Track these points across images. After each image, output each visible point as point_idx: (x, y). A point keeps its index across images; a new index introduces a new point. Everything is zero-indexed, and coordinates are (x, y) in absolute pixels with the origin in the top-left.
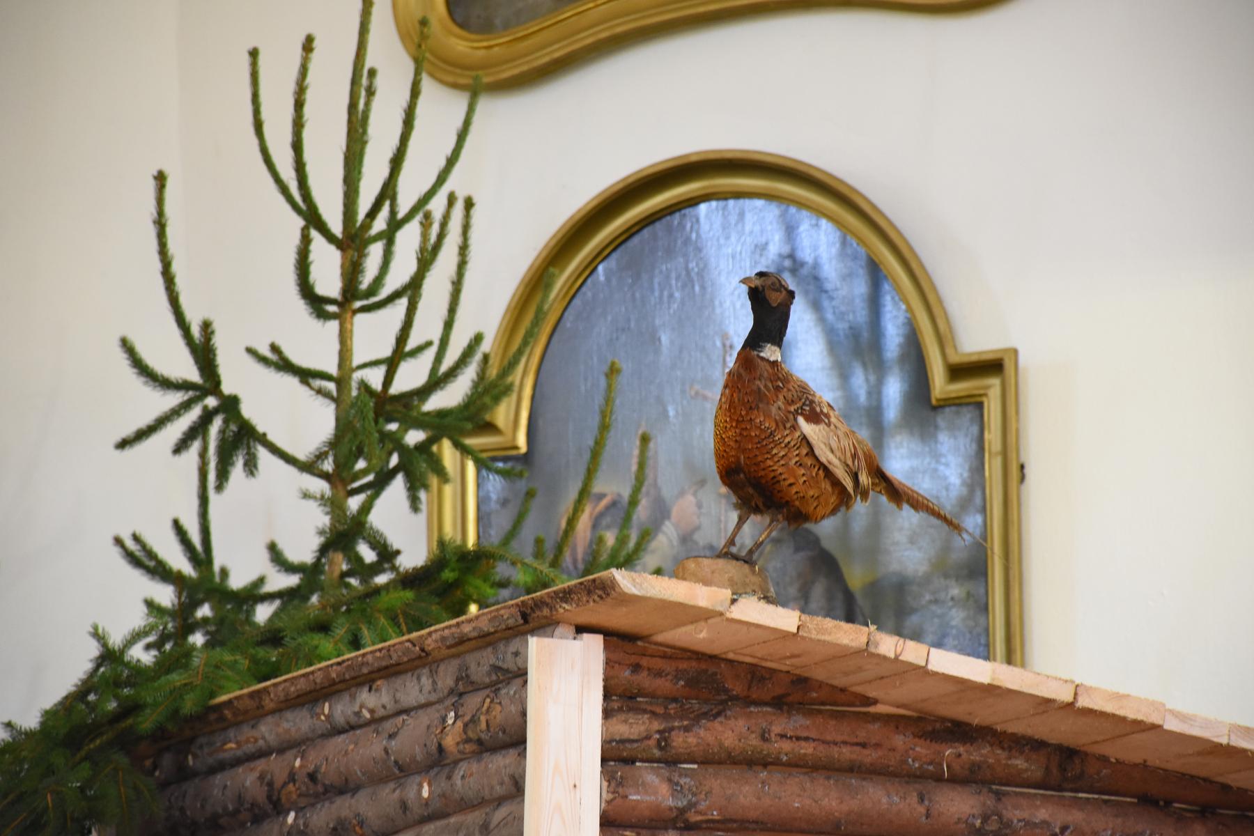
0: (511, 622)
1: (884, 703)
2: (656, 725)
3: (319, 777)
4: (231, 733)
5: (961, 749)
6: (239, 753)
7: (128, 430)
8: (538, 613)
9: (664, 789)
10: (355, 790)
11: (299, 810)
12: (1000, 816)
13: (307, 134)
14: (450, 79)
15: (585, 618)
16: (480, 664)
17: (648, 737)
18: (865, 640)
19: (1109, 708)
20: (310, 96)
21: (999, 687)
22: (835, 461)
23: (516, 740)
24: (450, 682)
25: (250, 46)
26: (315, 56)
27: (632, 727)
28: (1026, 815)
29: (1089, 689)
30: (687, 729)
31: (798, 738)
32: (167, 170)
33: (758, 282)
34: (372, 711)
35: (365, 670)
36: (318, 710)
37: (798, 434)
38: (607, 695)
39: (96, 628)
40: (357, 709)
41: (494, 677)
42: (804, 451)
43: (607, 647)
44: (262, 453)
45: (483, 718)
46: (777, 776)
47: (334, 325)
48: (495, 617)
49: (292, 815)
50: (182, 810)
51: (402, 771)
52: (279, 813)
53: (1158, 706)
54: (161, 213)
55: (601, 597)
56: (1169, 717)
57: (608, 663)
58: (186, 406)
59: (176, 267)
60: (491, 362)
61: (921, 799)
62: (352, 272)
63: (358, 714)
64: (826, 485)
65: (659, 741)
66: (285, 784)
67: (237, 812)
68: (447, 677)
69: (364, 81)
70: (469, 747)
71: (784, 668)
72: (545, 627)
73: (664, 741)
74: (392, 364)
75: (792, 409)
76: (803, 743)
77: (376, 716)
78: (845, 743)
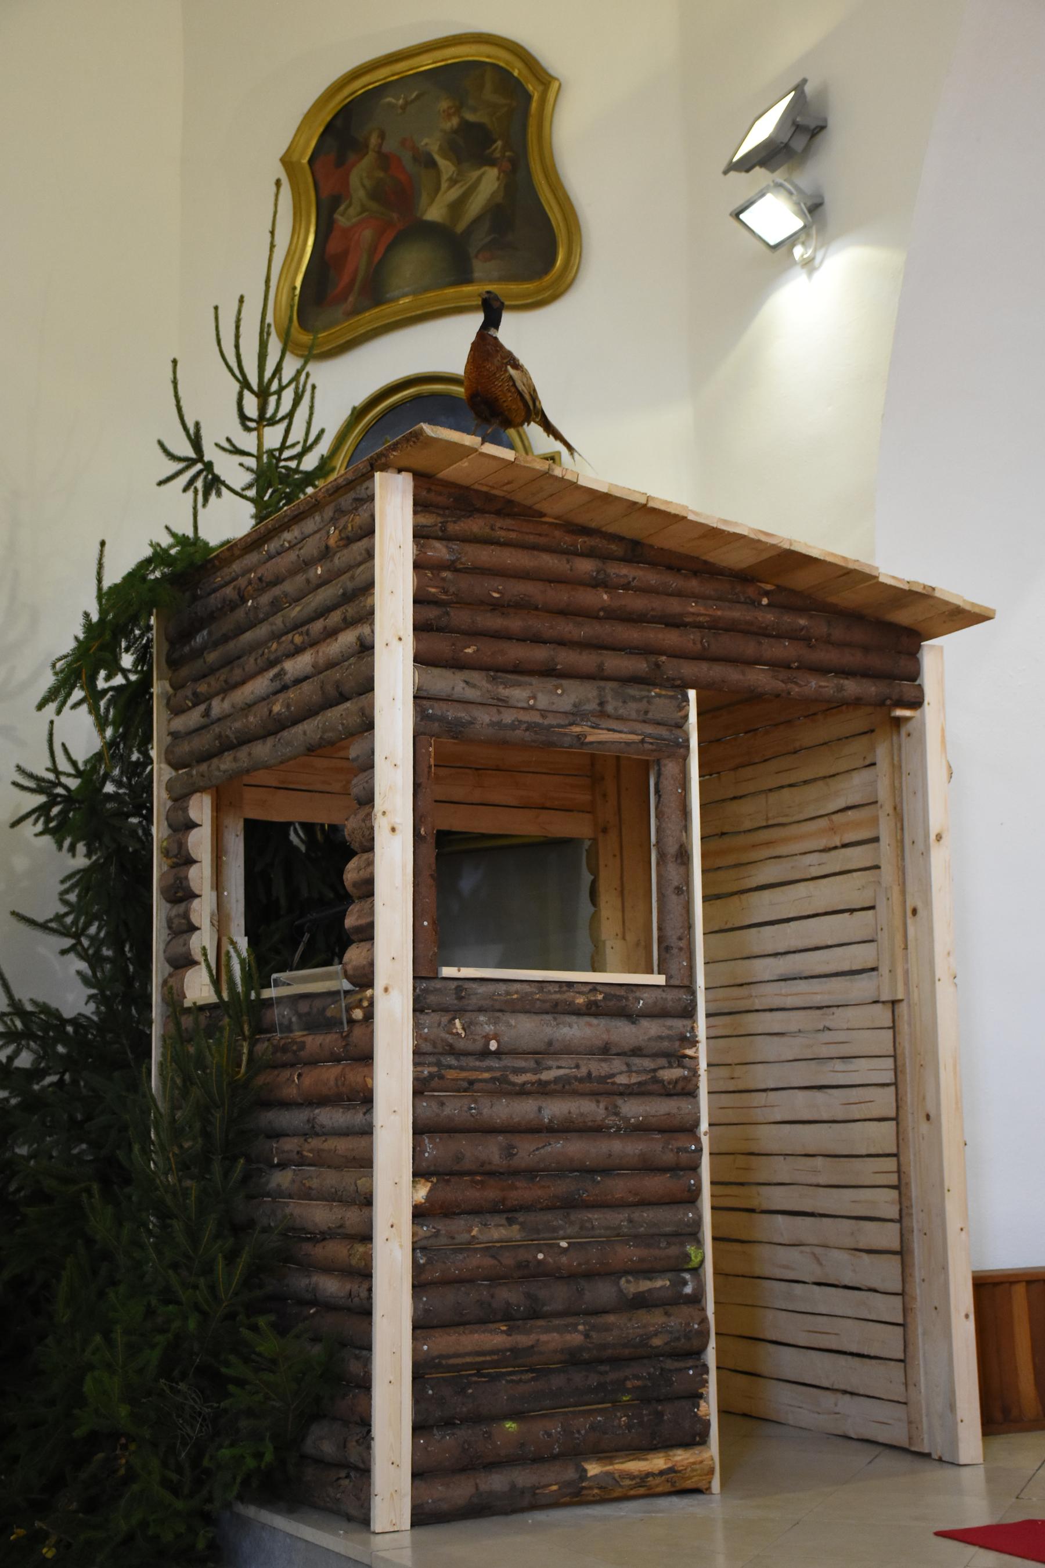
0: (364, 471)
1: (550, 517)
2: (440, 519)
3: (264, 578)
4: (218, 574)
5: (586, 539)
6: (222, 582)
7: (163, 477)
8: (379, 462)
9: (444, 550)
10: (283, 580)
11: (253, 599)
12: (605, 571)
13: (241, 341)
14: (300, 353)
15: (403, 463)
16: (346, 501)
17: (436, 525)
18: (547, 467)
19: (663, 507)
20: (242, 323)
21: (611, 495)
22: (526, 391)
23: (369, 531)
24: (331, 514)
25: (215, 304)
26: (245, 305)
27: (427, 520)
28: (617, 571)
29: (653, 498)
30: (455, 522)
31: (509, 530)
32: (178, 359)
33: (486, 296)
34: (289, 542)
35: (286, 520)
36: (261, 550)
37: (507, 374)
38: (415, 505)
39: (151, 542)
40: (281, 543)
41: (354, 505)
42: (511, 384)
43: (414, 479)
44: (224, 490)
45: (350, 525)
46: (499, 548)
47: (255, 434)
48: (356, 470)
49: (251, 601)
50: (196, 613)
51: (308, 564)
52: (243, 603)
53: (685, 508)
54: (175, 378)
55: (414, 442)
56: (690, 513)
57: (416, 487)
58: (187, 468)
59: (182, 403)
60: (209, 952)
61: (568, 562)
62: (262, 408)
63: (282, 545)
64: (520, 404)
65: (441, 527)
66: (247, 586)
67: (223, 607)
68: (329, 512)
69: (266, 330)
70: (341, 543)
71: (501, 494)
72: (384, 468)
73: (443, 530)
74: (283, 447)
75: (505, 361)
76: (511, 533)
77: (292, 544)
78: (531, 533)
